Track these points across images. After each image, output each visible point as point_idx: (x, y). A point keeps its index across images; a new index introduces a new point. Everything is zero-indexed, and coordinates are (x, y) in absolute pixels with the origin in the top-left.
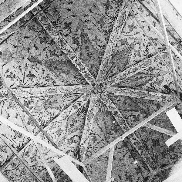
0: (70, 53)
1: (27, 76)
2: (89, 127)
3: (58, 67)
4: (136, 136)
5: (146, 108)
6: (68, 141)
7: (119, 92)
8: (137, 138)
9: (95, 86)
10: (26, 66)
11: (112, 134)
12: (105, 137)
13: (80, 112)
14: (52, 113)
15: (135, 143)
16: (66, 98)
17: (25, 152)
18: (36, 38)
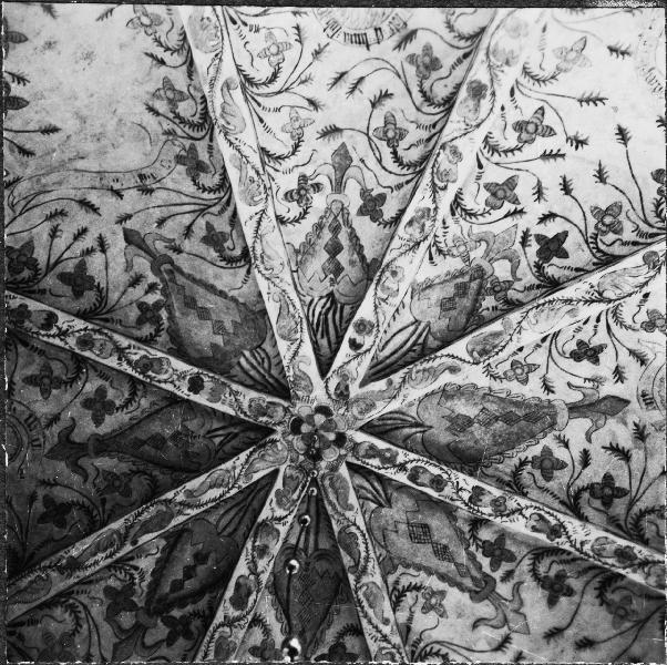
0: (499, 507)
1: (601, 348)
2: (272, 286)
3: (499, 425)
4: (67, 347)
5: (92, 472)
6: (317, 187)
7: (237, 471)
8: (57, 341)
9: (332, 437)
10: (619, 374)
11: (152, 288)
12: (171, 262)
13: (331, 312)
14: (437, 258)
15: (50, 320)
16: (414, 338)
17: (489, 92)
18: (635, 484)
